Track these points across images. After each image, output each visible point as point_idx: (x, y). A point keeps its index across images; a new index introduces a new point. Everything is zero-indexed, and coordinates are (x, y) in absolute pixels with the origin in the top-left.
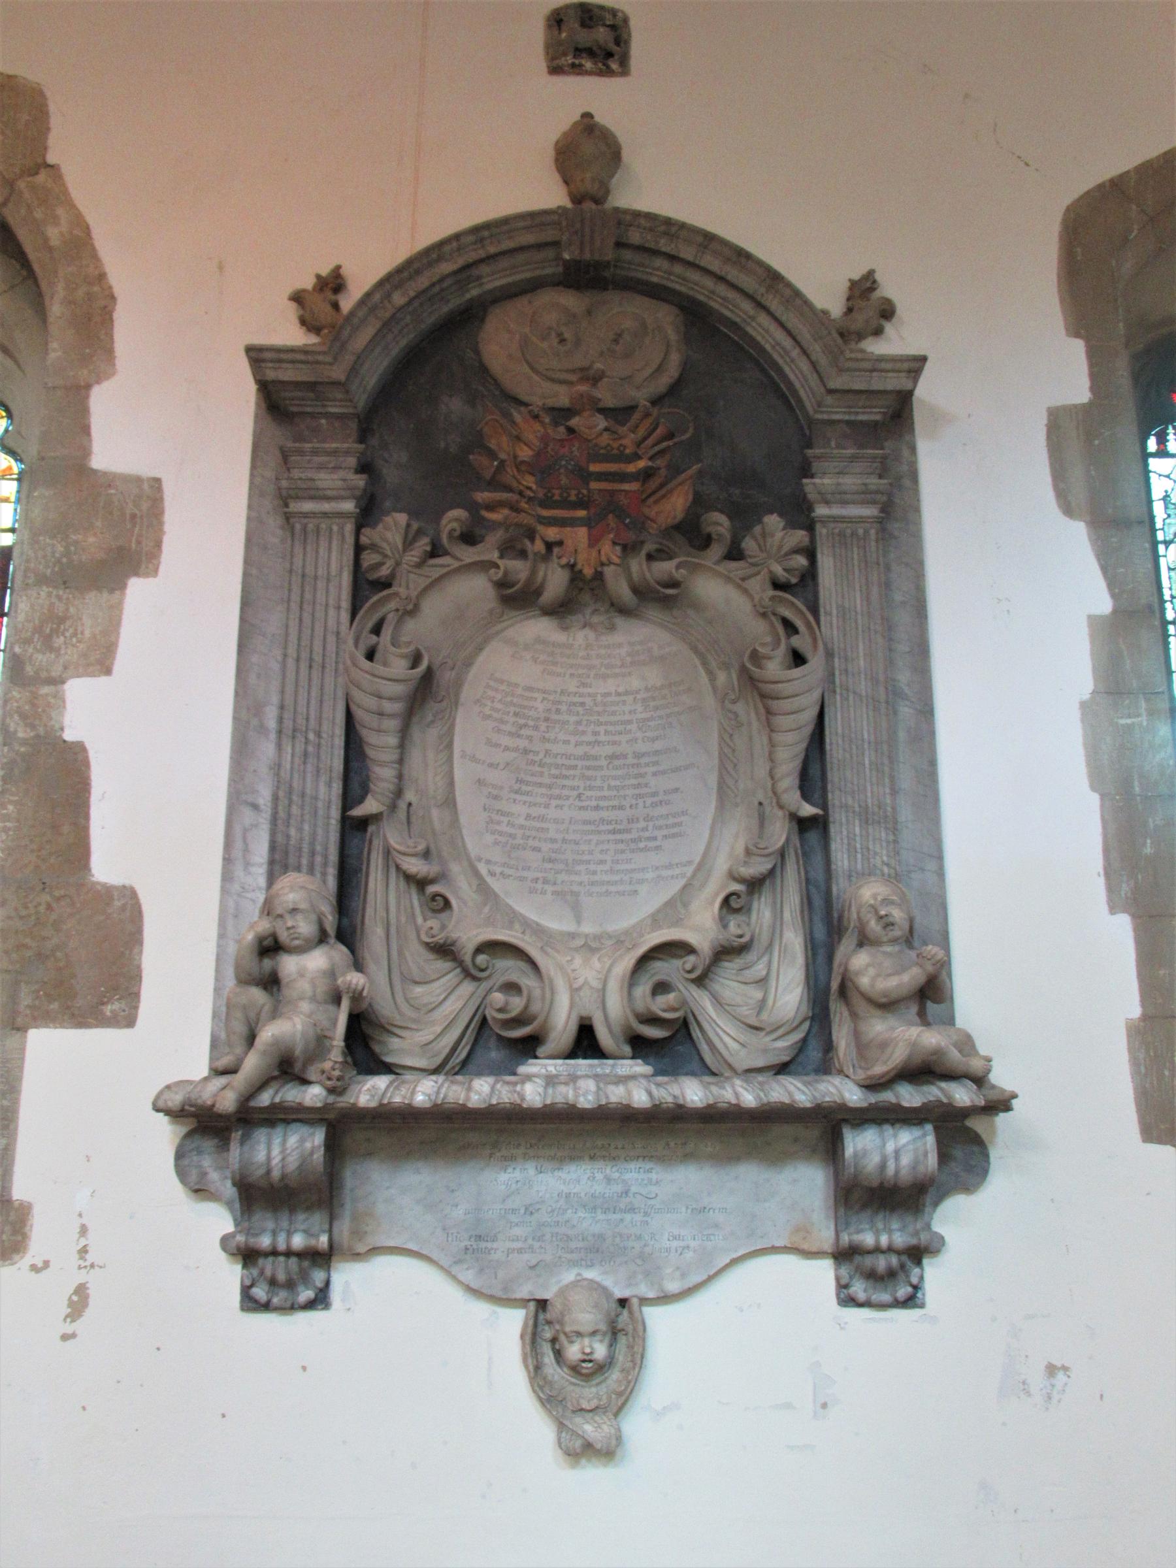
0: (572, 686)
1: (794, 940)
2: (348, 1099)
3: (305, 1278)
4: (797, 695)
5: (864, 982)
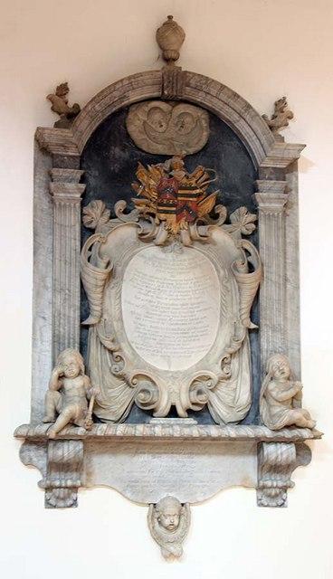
0: (168, 276)
1: (247, 376)
2: (93, 433)
3: (69, 496)
4: (302, 428)
5: (274, 394)
